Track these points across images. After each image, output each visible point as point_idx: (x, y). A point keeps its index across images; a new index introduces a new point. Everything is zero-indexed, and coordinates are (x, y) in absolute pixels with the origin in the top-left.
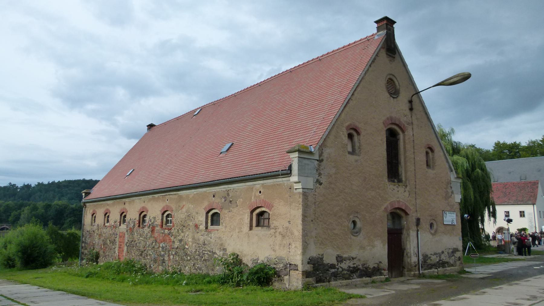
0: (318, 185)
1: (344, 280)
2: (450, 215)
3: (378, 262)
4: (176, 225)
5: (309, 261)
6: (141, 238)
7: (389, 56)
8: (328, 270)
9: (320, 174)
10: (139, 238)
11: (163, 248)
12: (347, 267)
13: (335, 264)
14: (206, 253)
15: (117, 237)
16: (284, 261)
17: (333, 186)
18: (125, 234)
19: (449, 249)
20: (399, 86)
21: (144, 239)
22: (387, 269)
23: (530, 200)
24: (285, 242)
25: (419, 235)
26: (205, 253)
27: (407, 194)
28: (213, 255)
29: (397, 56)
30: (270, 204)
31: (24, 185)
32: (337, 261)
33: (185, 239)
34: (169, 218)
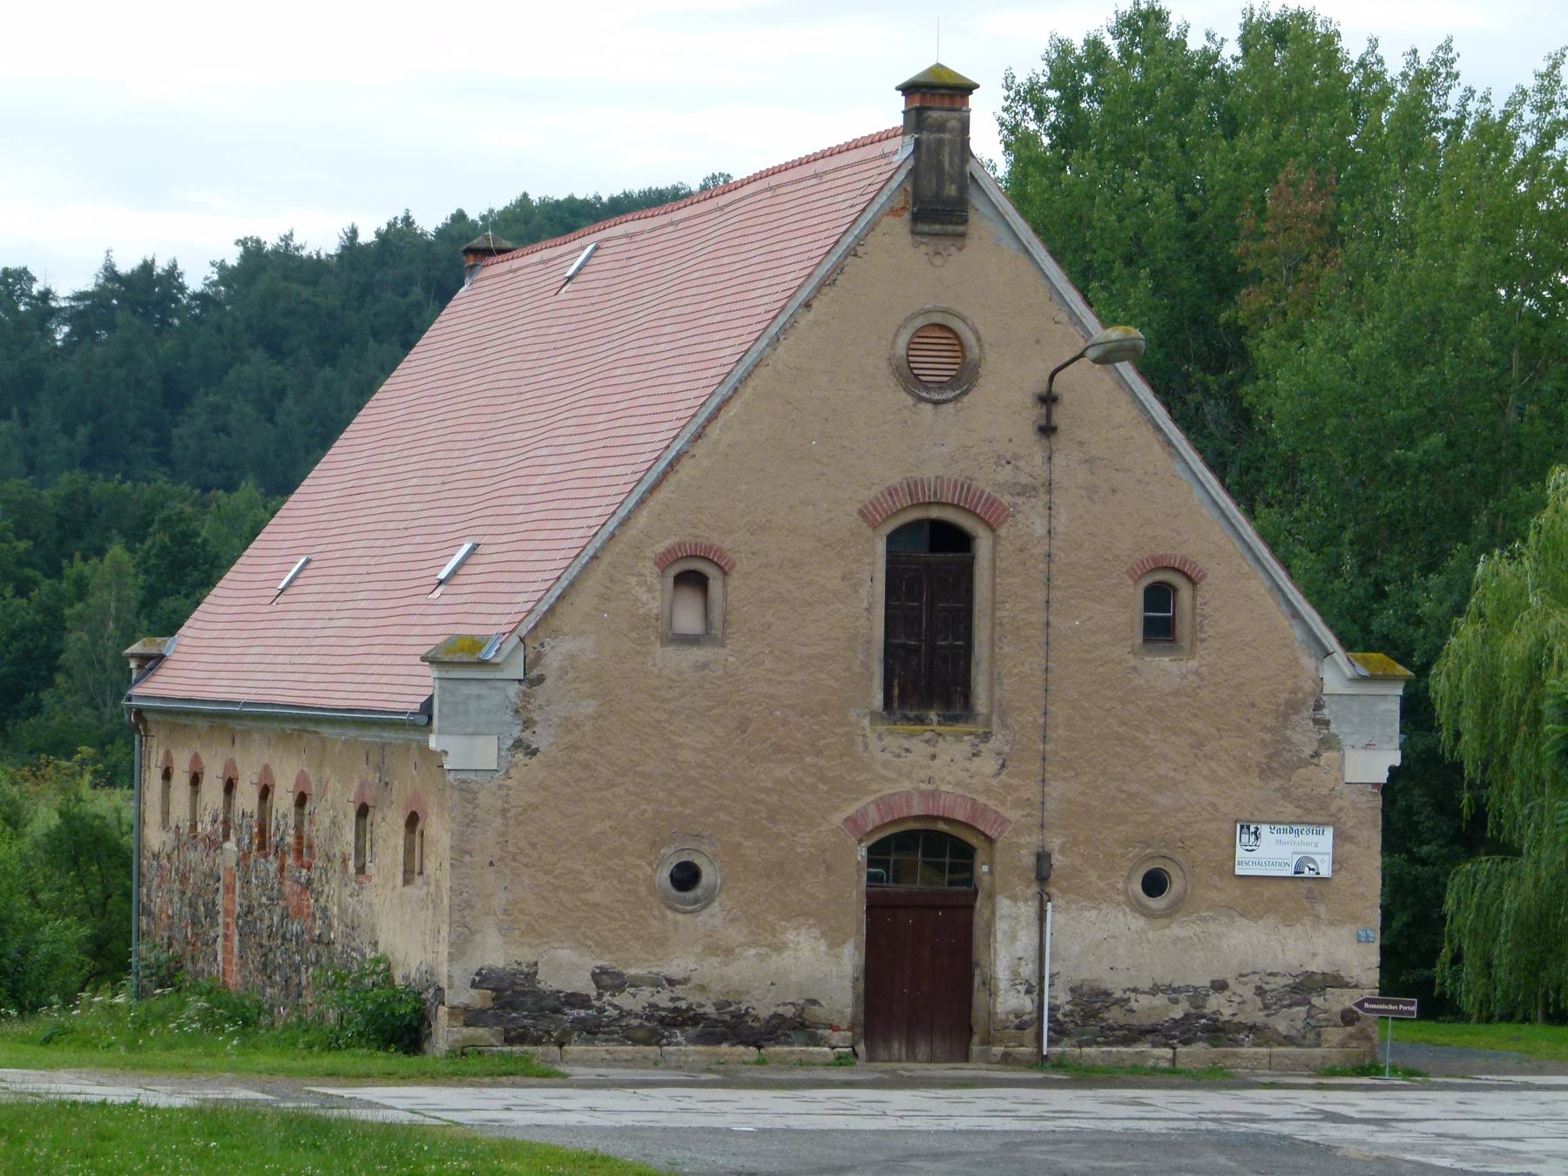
1: (626, 1045)
5: (477, 978)
8: (557, 1011)
9: (528, 724)
12: (644, 1008)
13: (588, 996)
17: (583, 756)
20: (981, 347)
31: (111, 273)
32: (599, 987)
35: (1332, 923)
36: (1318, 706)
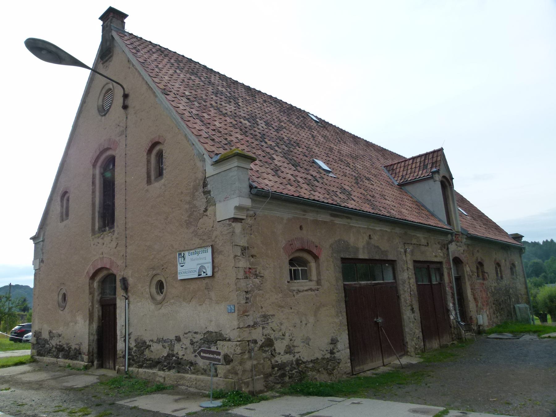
19: (196, 333)
35: (217, 303)
36: (205, 185)
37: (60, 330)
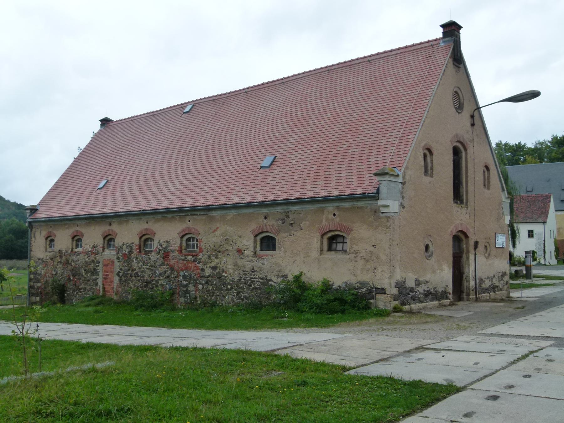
0: (402, 208)
2: (501, 237)
3: (445, 286)
4: (205, 250)
6: (144, 267)
7: (455, 67)
9: (403, 197)
10: (141, 266)
11: (184, 276)
14: (257, 281)
15: (99, 265)
16: (369, 285)
18: (113, 262)
19: (499, 273)
20: (463, 99)
21: (151, 267)
22: (452, 293)
23: (541, 217)
24: (368, 266)
25: (477, 258)
26: (254, 281)
27: (468, 216)
28: (268, 283)
29: (461, 66)
30: (348, 228)
32: (416, 285)
33: (221, 266)
34: (190, 242)
37: (428, 277)
